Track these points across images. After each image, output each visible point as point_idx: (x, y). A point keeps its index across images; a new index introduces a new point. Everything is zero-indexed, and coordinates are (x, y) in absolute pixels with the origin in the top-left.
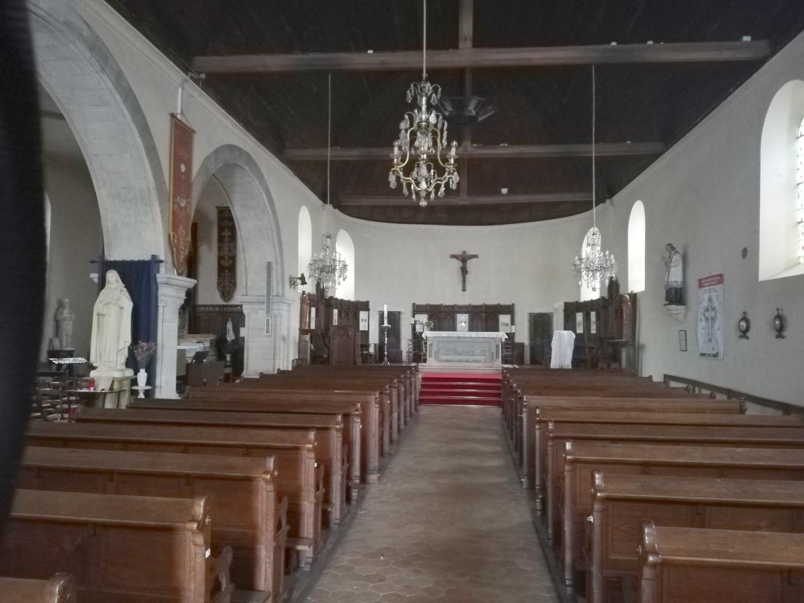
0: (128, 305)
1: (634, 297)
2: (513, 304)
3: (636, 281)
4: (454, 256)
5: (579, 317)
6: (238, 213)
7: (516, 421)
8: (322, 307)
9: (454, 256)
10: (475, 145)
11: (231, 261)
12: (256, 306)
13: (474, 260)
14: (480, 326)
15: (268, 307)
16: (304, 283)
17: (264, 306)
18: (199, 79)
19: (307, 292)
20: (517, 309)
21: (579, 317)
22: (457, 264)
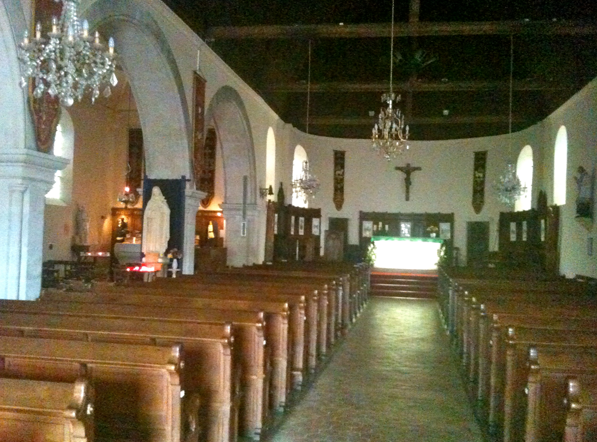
0: (167, 211)
1: (557, 209)
2: (453, 214)
3: (560, 196)
4: (398, 168)
5: (513, 226)
6: (221, 134)
7: (453, 321)
8: (282, 213)
9: (398, 168)
10: (420, 80)
11: (210, 174)
12: (234, 212)
13: (417, 172)
14: (421, 233)
15: (244, 213)
16: (271, 193)
17: (241, 213)
18: (211, 42)
19: (272, 201)
20: (456, 218)
21: (513, 226)
22: (402, 175)
